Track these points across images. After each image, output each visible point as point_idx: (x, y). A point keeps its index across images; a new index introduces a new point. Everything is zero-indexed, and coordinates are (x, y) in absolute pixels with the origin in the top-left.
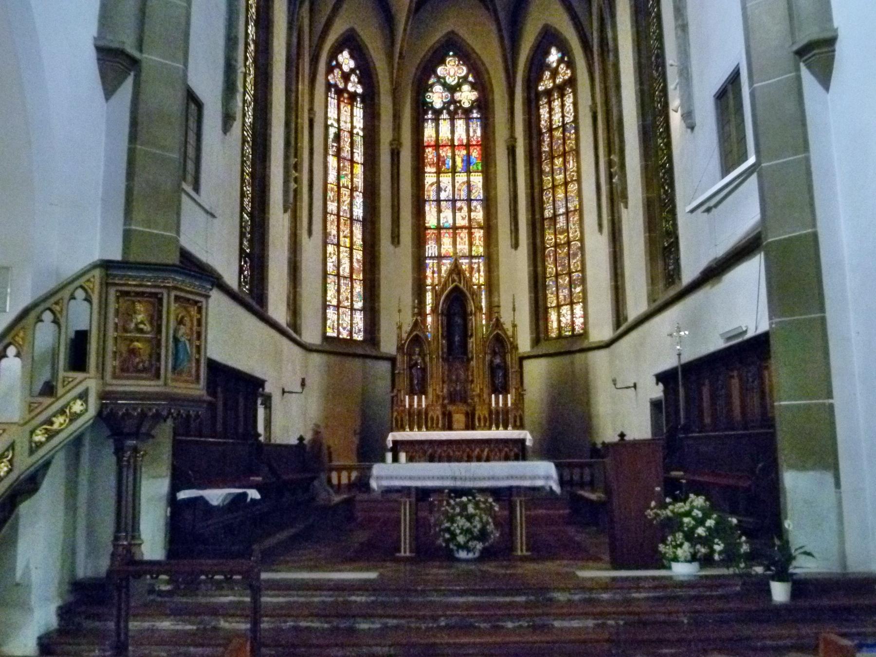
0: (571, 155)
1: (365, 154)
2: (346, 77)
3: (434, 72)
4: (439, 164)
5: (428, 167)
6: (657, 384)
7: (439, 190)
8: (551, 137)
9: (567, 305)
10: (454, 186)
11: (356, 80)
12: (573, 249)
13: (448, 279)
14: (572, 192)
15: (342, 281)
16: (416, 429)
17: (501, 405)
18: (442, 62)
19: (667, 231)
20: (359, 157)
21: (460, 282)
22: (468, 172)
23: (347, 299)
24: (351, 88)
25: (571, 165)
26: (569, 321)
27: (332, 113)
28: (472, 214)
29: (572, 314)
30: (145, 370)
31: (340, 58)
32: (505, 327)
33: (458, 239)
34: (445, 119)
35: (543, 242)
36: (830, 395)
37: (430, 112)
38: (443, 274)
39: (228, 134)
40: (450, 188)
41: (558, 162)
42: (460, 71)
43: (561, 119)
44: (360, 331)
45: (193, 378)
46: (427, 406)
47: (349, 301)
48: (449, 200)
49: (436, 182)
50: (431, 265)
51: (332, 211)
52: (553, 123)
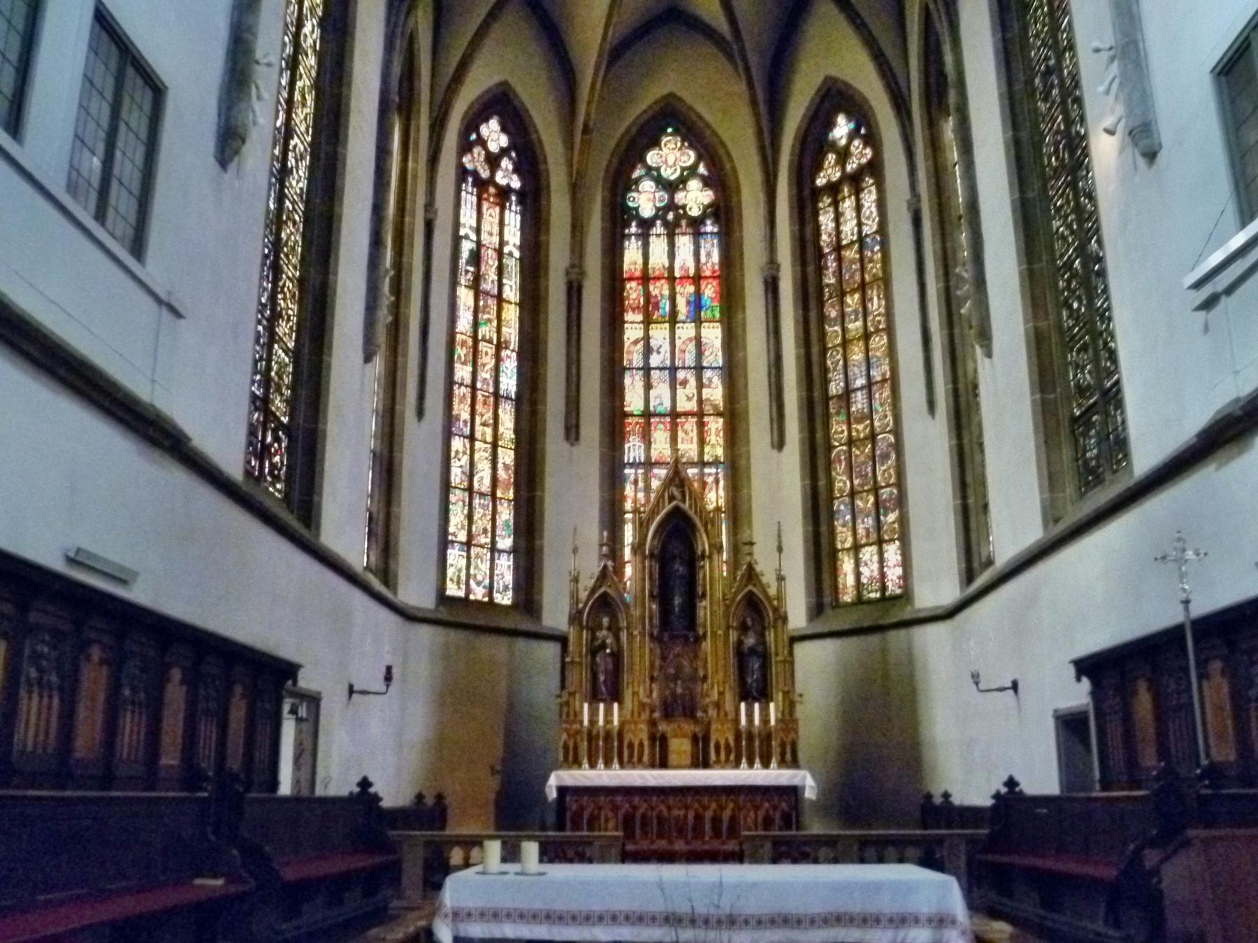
0: (875, 287)
1: (523, 289)
2: (493, 161)
3: (642, 160)
4: (648, 308)
6: (1078, 679)
7: (648, 351)
8: (839, 259)
9: (871, 545)
11: (511, 167)
12: (881, 447)
13: (662, 496)
15: (477, 501)
16: (601, 765)
17: (757, 721)
18: (655, 143)
19: (1078, 386)
20: (512, 291)
21: (684, 500)
22: (698, 321)
23: (485, 531)
24: (500, 178)
25: (876, 305)
26: (876, 574)
27: (468, 217)
28: (705, 391)
29: (882, 560)
31: (484, 130)
32: (764, 580)
33: (680, 434)
34: (658, 235)
37: (634, 224)
39: (232, 167)
40: (666, 347)
41: (853, 301)
42: (684, 158)
43: (856, 229)
44: (506, 588)
46: (622, 724)
47: (489, 535)
49: (643, 339)
51: (463, 379)
52: (843, 236)
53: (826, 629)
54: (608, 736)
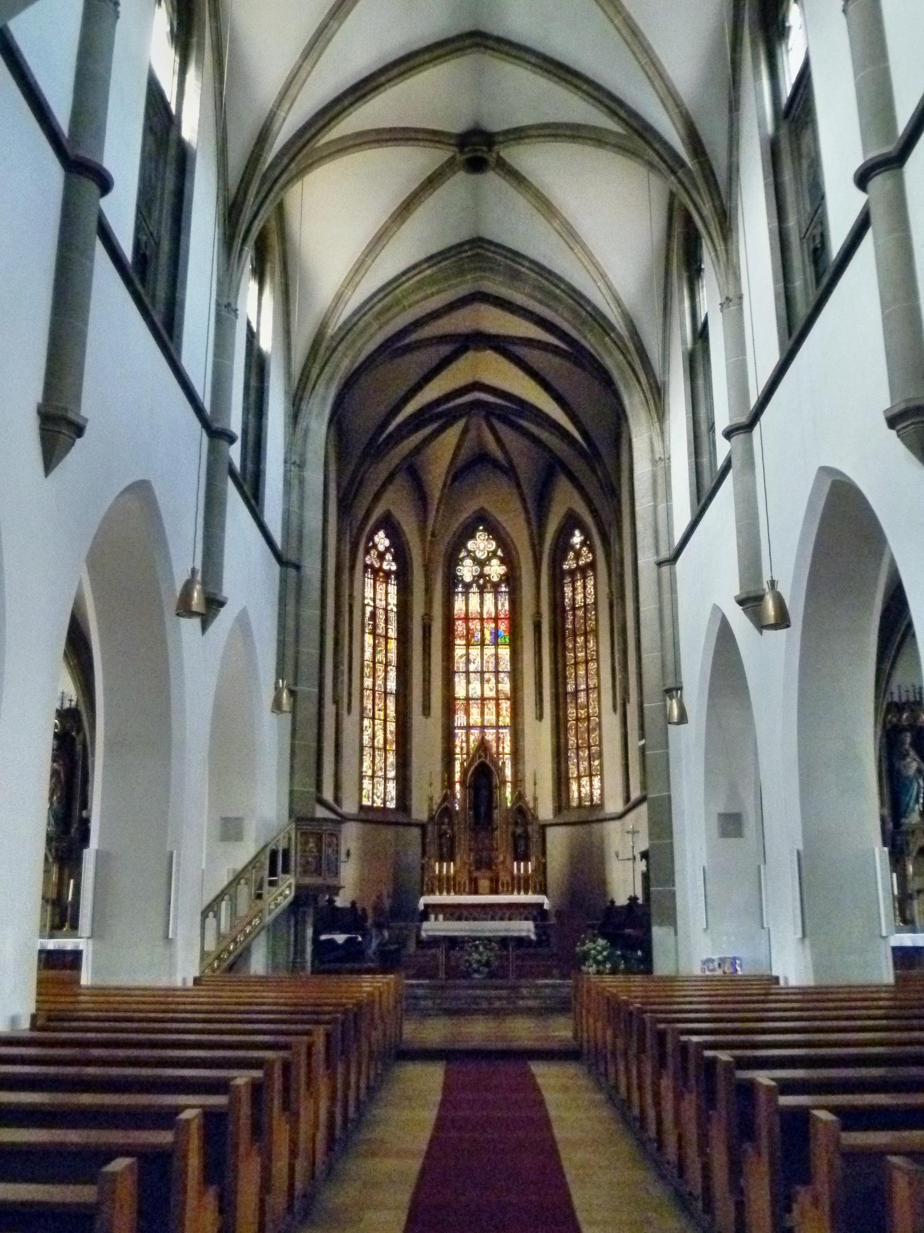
2: (381, 556)
7: (468, 661)
8: (574, 615)
10: (482, 658)
16: (445, 893)
17: (522, 871)
18: (472, 537)
20: (393, 633)
21: (486, 758)
22: (496, 644)
23: (381, 769)
24: (386, 566)
25: (591, 644)
26: (588, 792)
27: (369, 593)
29: (591, 785)
31: (376, 539)
33: (486, 710)
34: (474, 593)
35: (566, 715)
36: (673, 885)
38: (472, 745)
40: (479, 659)
41: (580, 640)
44: (392, 799)
46: (455, 872)
53: (562, 821)
54: (448, 878)
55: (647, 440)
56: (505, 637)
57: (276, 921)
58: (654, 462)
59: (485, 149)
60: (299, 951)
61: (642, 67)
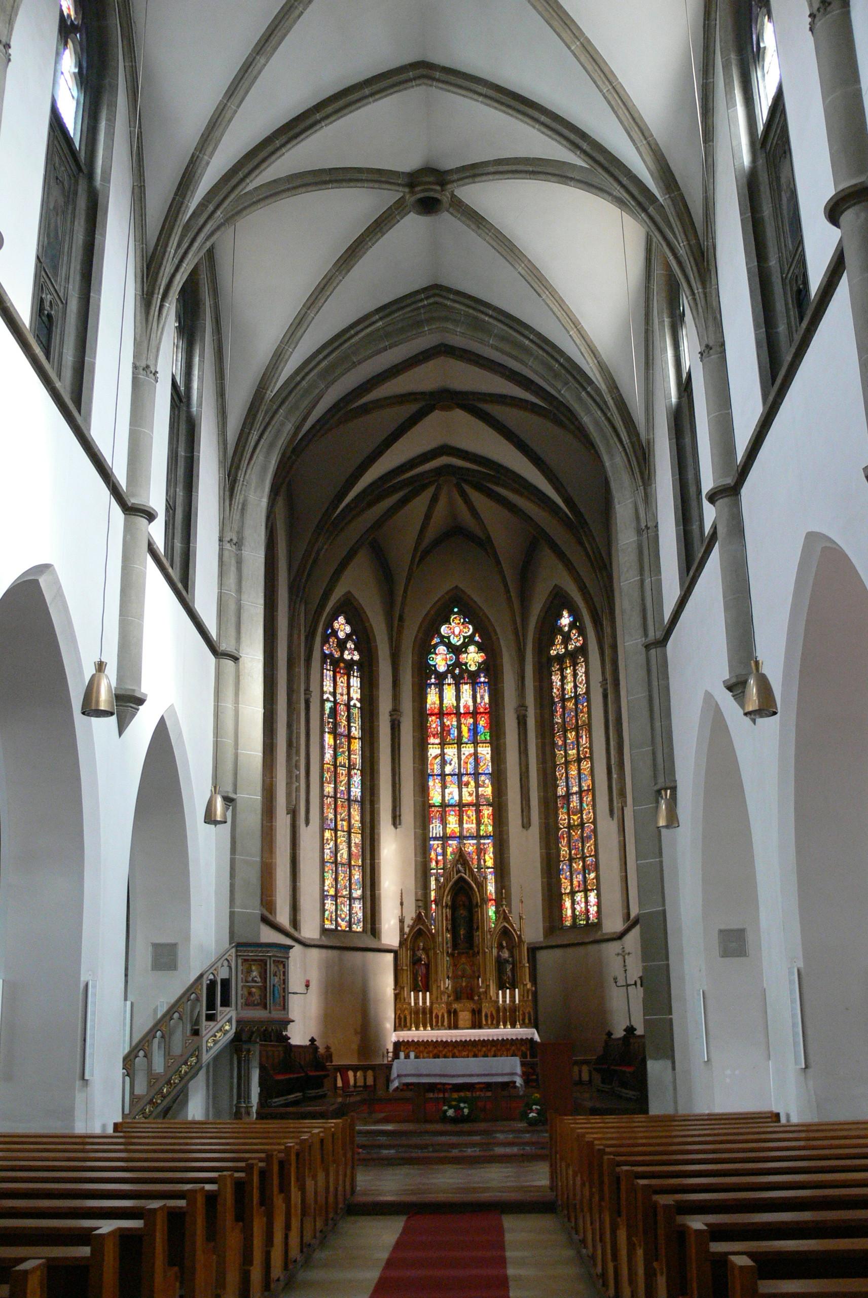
2: (342, 645)
5: (432, 738)
7: (444, 763)
8: (564, 708)
9: (580, 892)
10: (459, 758)
11: (353, 646)
14: (585, 770)
17: (508, 1002)
18: (447, 621)
20: (356, 732)
22: (475, 743)
23: (345, 888)
24: (347, 656)
25: (584, 740)
26: (583, 909)
27: (328, 686)
28: (480, 789)
29: (587, 902)
30: (258, 1005)
33: (465, 818)
34: (449, 684)
36: (670, 1013)
38: (449, 857)
40: (455, 760)
41: (571, 736)
44: (359, 921)
45: (282, 1008)
48: (455, 775)
49: (440, 755)
50: (435, 846)
51: (329, 793)
55: (631, 506)
56: (484, 734)
57: (216, 1058)
58: (639, 532)
59: (438, 188)
60: (243, 1093)
61: (604, 95)
